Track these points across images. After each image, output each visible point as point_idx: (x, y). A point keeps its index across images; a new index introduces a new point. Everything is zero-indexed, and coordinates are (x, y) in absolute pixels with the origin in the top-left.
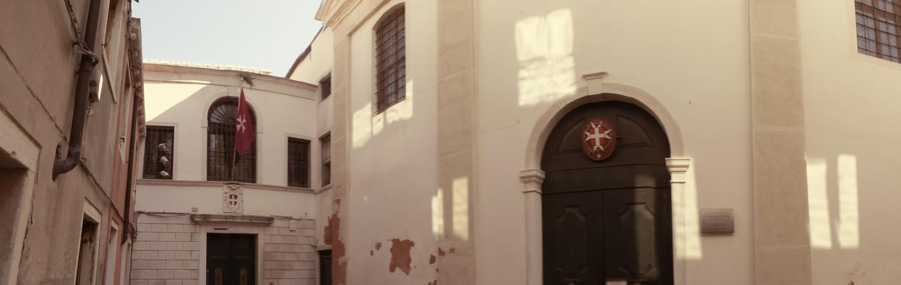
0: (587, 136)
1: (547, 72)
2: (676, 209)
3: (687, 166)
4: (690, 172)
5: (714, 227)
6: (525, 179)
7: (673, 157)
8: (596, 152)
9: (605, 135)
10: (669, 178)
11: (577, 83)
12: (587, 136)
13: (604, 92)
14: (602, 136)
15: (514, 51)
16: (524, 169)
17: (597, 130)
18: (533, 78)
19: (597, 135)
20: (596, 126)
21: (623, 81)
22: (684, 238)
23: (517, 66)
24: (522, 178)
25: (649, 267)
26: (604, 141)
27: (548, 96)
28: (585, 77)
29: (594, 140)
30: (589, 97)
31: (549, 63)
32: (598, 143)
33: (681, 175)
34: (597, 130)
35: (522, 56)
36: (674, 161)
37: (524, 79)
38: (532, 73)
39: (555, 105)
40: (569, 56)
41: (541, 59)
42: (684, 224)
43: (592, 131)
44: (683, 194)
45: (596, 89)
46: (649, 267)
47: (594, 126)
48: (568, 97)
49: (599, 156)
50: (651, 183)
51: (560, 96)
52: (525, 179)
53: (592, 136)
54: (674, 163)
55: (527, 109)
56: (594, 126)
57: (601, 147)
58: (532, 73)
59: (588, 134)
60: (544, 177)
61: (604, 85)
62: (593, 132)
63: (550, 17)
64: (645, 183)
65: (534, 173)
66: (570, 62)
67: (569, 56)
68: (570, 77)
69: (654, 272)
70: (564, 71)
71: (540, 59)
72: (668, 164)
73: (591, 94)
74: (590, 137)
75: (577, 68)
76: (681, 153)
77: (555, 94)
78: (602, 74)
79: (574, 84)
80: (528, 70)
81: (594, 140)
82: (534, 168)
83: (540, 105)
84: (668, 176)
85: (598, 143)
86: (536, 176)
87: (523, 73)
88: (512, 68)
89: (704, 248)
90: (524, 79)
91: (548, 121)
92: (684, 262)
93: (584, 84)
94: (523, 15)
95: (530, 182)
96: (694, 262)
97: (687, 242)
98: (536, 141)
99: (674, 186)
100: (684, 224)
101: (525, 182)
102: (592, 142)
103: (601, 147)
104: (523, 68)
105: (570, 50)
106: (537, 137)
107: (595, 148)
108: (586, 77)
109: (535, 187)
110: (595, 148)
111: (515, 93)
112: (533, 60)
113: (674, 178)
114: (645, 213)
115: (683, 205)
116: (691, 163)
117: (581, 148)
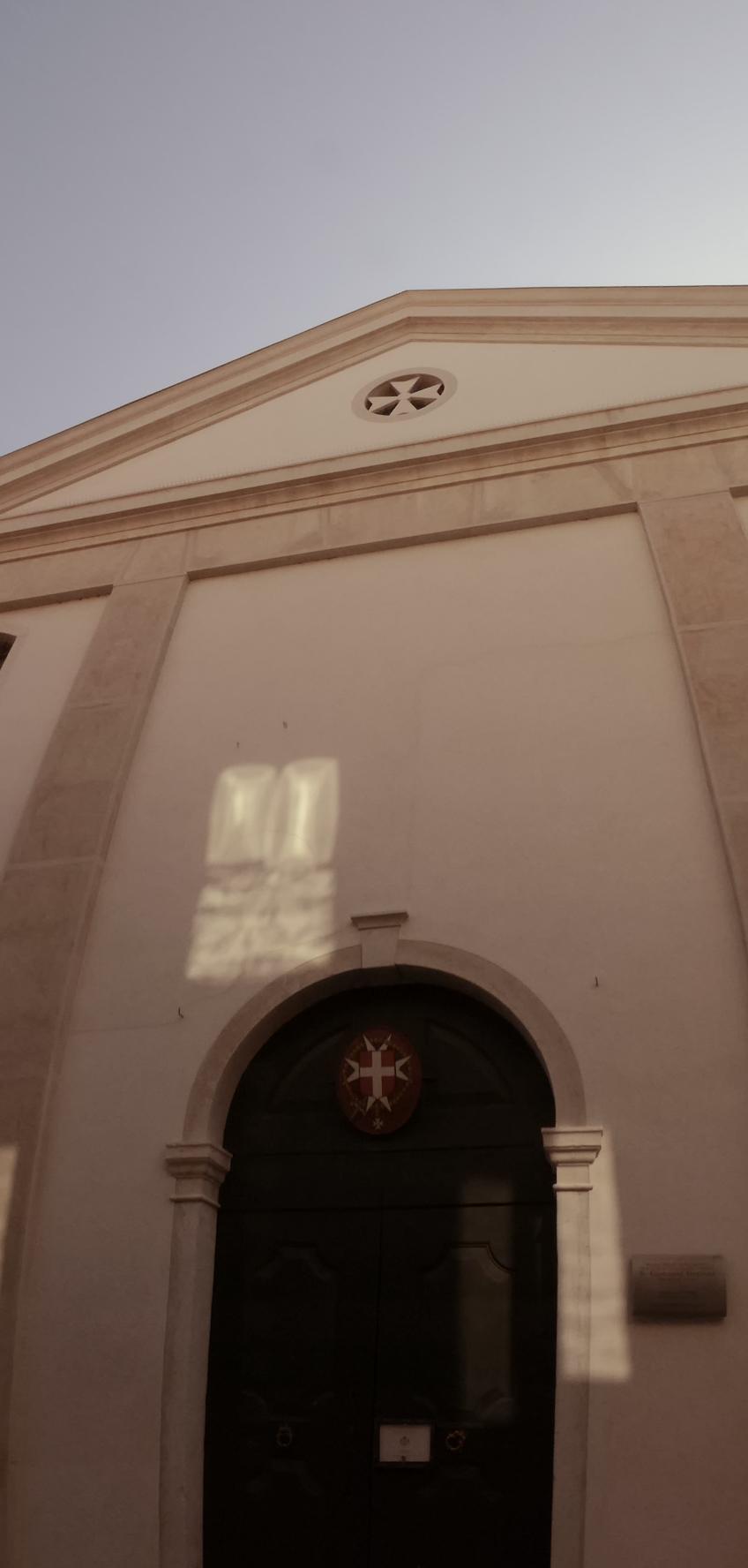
0: (351, 1070)
2: (568, 1258)
3: (596, 1149)
4: (602, 1164)
6: (178, 1168)
7: (559, 1127)
10: (553, 1178)
11: (336, 934)
12: (351, 1070)
13: (399, 962)
14: (389, 1071)
15: (201, 838)
16: (177, 1139)
17: (377, 1057)
18: (236, 912)
19: (377, 1070)
20: (377, 1046)
21: (460, 929)
22: (586, 1329)
26: (392, 1086)
27: (258, 961)
28: (357, 921)
31: (273, 879)
33: (580, 1170)
34: (377, 1057)
35: (216, 854)
36: (563, 1137)
37: (212, 911)
38: (234, 899)
40: (321, 867)
42: (587, 1295)
43: (365, 1060)
44: (584, 1222)
45: (381, 953)
47: (370, 1047)
48: (308, 969)
49: (378, 1123)
50: (503, 1194)
51: (288, 967)
52: (178, 1168)
53: (366, 1072)
54: (562, 1141)
55: (206, 989)
56: (370, 1047)
57: (385, 1101)
58: (234, 899)
59: (354, 1064)
60: (228, 1167)
61: (402, 944)
63: (290, 770)
64: (485, 1210)
65: (205, 1153)
66: (322, 884)
67: (321, 867)
70: (306, 904)
71: (253, 868)
72: (547, 1142)
73: (365, 966)
74: (359, 1072)
75: (338, 900)
76: (579, 1117)
77: (277, 960)
78: (399, 918)
79: (326, 939)
80: (226, 890)
81: (370, 1080)
82: (205, 1140)
83: (238, 984)
84: (548, 1173)
87: (212, 897)
88: (187, 876)
89: (636, 1354)
90: (212, 911)
91: (262, 1015)
92: (585, 1387)
93: (353, 939)
94: (244, 752)
95: (189, 1176)
96: (610, 1388)
97: (594, 1337)
99: (562, 1198)
100: (587, 1295)
101: (179, 1177)
102: (362, 1087)
103: (385, 1101)
104: (213, 881)
105: (327, 856)
106: (226, 1057)
107: (371, 1101)
108: (359, 922)
111: (181, 941)
112: (242, 867)
113: (565, 1178)
114: (485, 1269)
116: (604, 1142)
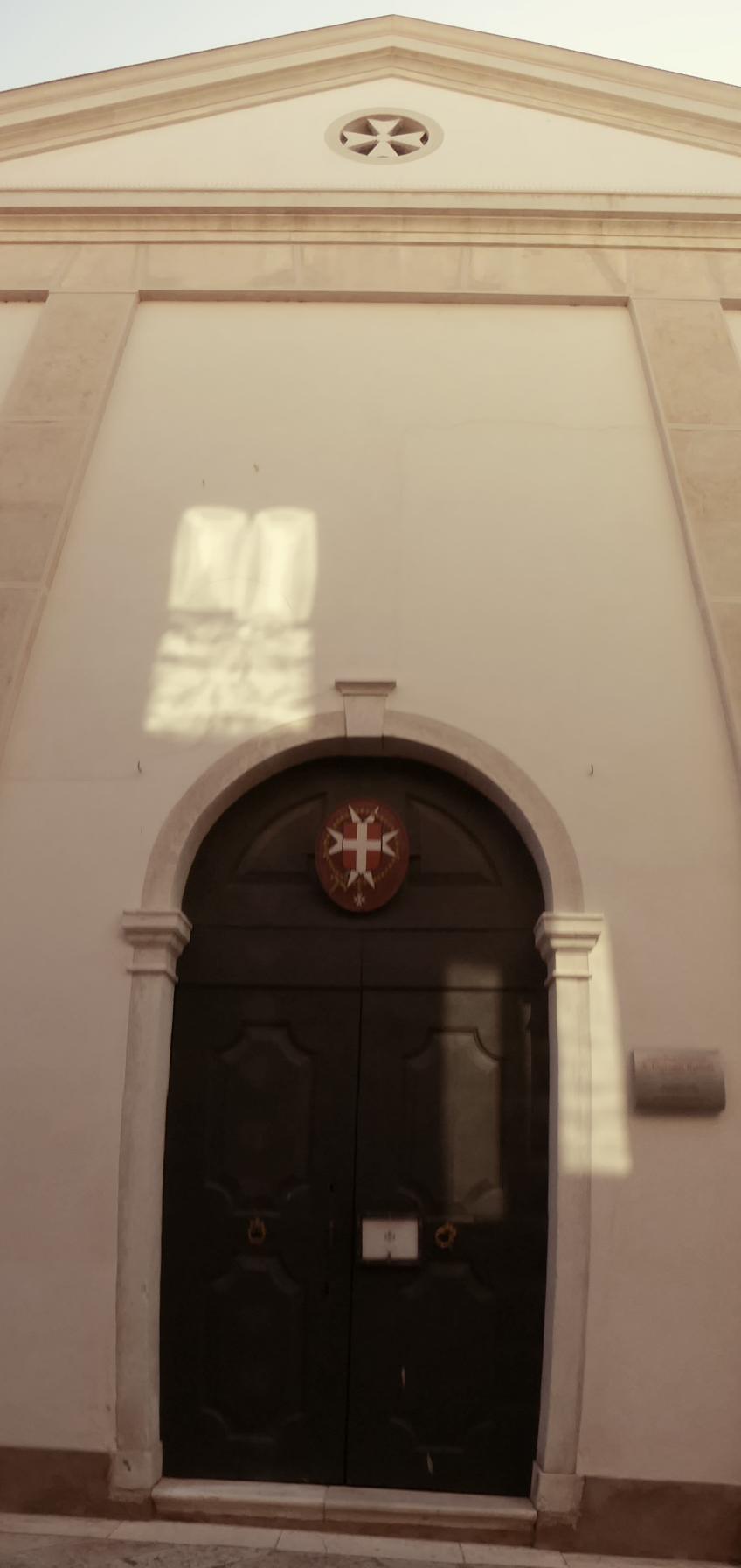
0: (333, 842)
1: (239, 646)
3: (595, 937)
5: (669, 1096)
6: (138, 937)
8: (354, 886)
9: (381, 845)
11: (314, 699)
12: (333, 842)
13: (387, 733)
14: (375, 845)
15: (161, 577)
16: (136, 905)
17: (362, 829)
18: (202, 664)
19: (362, 842)
20: (363, 817)
22: (587, 1122)
23: (161, 620)
24: (129, 932)
25: (480, 1189)
27: (228, 719)
28: (340, 685)
29: (352, 855)
30: (344, 741)
31: (244, 632)
32: (361, 864)
33: (578, 958)
34: (362, 829)
35: (179, 598)
36: (561, 922)
37: (174, 660)
38: (199, 650)
39: (249, 745)
40: (298, 625)
41: (227, 617)
43: (349, 831)
45: (367, 721)
46: (480, 1189)
47: (355, 817)
48: (283, 732)
49: (359, 900)
51: (263, 729)
52: (138, 937)
53: (349, 845)
55: (168, 743)
56: (355, 817)
57: (369, 877)
58: (199, 650)
59: (337, 836)
61: (389, 715)
62: (351, 833)
63: (263, 518)
66: (299, 644)
67: (298, 625)
68: (295, 682)
69: (491, 1203)
70: (281, 664)
74: (342, 844)
75: (317, 661)
76: (577, 903)
77: (249, 720)
80: (191, 639)
82: (167, 911)
83: (203, 743)
85: (361, 864)
86: (176, 933)
87: (174, 644)
88: (145, 617)
89: (636, 1147)
90: (174, 660)
92: (586, 1182)
93: (335, 703)
95: (151, 945)
96: (613, 1184)
97: (593, 1129)
98: (186, 835)
100: (587, 1088)
101: (137, 945)
103: (369, 877)
104: (177, 628)
105: (305, 613)
107: (353, 876)
109: (161, 961)
110: (353, 876)
111: (140, 691)
113: (563, 965)
115: (587, 1042)
117: (311, 873)
